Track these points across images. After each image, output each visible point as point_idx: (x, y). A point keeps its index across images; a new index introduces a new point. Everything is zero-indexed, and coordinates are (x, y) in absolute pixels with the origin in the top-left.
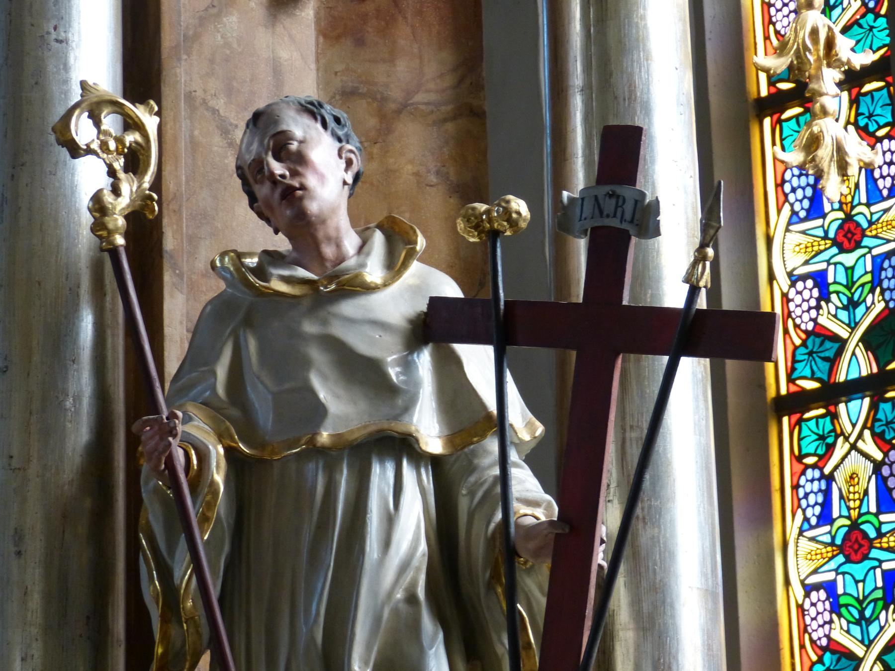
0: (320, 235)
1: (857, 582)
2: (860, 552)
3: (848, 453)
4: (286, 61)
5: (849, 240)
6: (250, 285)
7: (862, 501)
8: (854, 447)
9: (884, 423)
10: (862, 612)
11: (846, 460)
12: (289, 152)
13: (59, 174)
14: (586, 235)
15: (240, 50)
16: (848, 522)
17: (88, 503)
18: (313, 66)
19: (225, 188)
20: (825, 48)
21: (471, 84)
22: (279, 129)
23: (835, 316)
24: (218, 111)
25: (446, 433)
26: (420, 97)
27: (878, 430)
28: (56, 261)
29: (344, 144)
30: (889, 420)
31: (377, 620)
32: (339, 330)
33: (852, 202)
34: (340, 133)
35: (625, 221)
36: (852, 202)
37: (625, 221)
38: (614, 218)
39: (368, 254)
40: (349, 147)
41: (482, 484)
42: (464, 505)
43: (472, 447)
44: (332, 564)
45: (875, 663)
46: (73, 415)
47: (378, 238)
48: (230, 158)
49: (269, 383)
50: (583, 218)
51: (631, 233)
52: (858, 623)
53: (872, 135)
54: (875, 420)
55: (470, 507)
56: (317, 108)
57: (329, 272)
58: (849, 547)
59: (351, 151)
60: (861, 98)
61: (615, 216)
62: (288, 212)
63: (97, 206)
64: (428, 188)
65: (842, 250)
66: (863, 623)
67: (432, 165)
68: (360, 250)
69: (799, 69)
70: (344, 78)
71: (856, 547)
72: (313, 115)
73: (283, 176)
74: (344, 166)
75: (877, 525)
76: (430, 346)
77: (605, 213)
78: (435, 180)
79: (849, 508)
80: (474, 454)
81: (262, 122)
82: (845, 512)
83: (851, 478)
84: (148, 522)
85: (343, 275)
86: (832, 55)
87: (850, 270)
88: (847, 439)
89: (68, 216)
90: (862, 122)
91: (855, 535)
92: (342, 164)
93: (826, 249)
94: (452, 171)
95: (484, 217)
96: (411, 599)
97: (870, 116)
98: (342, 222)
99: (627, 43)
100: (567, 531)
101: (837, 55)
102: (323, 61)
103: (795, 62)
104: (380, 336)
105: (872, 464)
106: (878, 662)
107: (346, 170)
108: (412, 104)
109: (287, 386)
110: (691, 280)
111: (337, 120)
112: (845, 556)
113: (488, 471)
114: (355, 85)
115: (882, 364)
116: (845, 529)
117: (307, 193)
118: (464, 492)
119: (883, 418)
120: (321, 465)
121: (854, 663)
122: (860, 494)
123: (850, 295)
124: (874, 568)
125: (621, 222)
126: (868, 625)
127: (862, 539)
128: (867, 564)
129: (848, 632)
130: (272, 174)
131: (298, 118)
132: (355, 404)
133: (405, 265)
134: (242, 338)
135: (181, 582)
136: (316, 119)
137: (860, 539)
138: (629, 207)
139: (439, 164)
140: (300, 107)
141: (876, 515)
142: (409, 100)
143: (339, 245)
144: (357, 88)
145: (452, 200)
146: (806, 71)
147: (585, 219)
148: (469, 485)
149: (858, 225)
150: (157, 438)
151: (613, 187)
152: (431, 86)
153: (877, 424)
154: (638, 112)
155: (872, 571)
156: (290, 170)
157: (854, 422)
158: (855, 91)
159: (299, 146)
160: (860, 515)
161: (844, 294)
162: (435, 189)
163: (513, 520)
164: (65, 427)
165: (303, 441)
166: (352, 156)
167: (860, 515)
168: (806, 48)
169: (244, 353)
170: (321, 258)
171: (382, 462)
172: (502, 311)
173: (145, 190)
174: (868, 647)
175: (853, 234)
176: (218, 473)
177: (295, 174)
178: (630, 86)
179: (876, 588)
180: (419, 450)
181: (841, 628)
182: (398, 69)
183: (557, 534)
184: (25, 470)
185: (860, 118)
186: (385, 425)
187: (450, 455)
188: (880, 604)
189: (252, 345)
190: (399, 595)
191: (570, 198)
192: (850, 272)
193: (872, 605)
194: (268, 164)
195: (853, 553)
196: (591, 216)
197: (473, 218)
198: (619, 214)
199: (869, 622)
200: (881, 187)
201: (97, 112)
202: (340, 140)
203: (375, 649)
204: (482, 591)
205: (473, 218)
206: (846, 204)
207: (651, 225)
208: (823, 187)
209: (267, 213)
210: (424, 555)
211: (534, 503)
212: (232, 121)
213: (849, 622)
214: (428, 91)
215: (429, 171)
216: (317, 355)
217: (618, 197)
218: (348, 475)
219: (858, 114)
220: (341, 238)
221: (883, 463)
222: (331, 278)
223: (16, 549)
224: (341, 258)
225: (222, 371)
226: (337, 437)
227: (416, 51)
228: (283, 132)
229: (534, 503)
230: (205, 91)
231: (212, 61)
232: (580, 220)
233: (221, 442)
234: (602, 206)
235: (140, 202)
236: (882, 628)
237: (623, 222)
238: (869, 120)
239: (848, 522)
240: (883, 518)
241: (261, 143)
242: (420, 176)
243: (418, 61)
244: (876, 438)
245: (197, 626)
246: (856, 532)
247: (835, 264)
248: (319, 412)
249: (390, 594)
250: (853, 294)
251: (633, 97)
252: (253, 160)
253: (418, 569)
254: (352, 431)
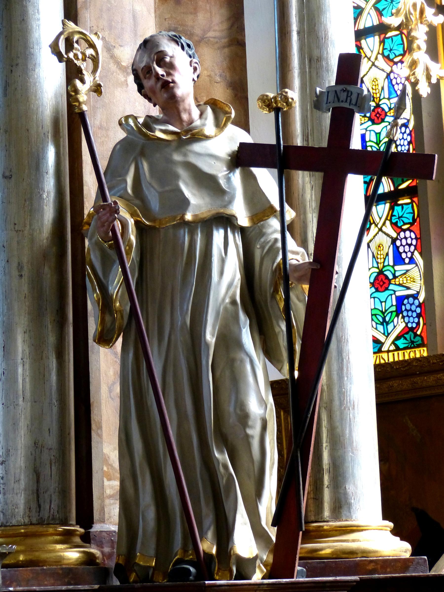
0: (181, 108)
1: (381, 302)
2: (383, 286)
3: (378, 233)
4: (139, 11)
5: (378, 118)
6: (145, 135)
7: (385, 259)
8: (380, 230)
9: (397, 217)
10: (384, 319)
11: (376, 236)
12: (165, 62)
13: (37, 70)
14: (330, 111)
15: (115, 5)
16: (377, 270)
17: (54, 249)
18: (153, 15)
19: (109, 81)
20: (419, 14)
21: (238, 27)
22: (160, 50)
23: (376, 329)
24: (105, 38)
25: (249, 215)
26: (211, 34)
27: (394, 221)
28: (36, 118)
29: (192, 59)
30: (400, 216)
31: (218, 313)
32: (193, 159)
33: (380, 97)
34: (190, 53)
35: (352, 104)
36: (380, 97)
37: (352, 104)
38: (346, 103)
39: (206, 119)
40: (195, 60)
41: (268, 242)
42: (258, 254)
43: (262, 223)
44: (194, 283)
45: (391, 345)
46: (48, 202)
47: (209, 111)
48: (112, 64)
49: (156, 186)
50: (328, 102)
51: (355, 111)
52: (382, 324)
53: (392, 60)
54: (392, 215)
55: (261, 255)
56: (179, 39)
57: (186, 128)
58: (377, 284)
59: (196, 63)
60: (386, 40)
61: (346, 101)
62: (165, 95)
63: (73, 89)
64: (215, 84)
65: (374, 123)
66: (385, 324)
67: (217, 72)
68: (201, 115)
69: (406, 25)
70: (170, 22)
71: (382, 283)
72: (177, 43)
73: (163, 75)
74: (193, 70)
75: (393, 272)
76: (239, 168)
77: (341, 100)
78: (219, 80)
79: (378, 263)
80: (263, 226)
81: (149, 46)
82: (375, 265)
83: (379, 246)
84: (90, 260)
85: (194, 130)
86: (423, 17)
87: (378, 134)
88: (376, 226)
89: (42, 94)
90: (386, 53)
91: (382, 277)
92: (192, 69)
93: (365, 123)
94: (228, 75)
95: (273, 100)
96: (233, 302)
97: (391, 50)
98: (190, 102)
99: (324, 8)
100: (319, 267)
101: (426, 18)
102: (158, 12)
103: (404, 21)
104: (215, 163)
105: (391, 239)
106: (392, 345)
107: (194, 73)
108: (207, 37)
109: (167, 188)
110: (390, 136)
111: (189, 46)
112: (375, 288)
113: (271, 236)
114: (176, 26)
115: (396, 186)
116: (376, 274)
117: (176, 85)
118: (258, 246)
119: (397, 215)
120: (187, 230)
121: (379, 345)
122: (384, 255)
123: (378, 148)
124: (391, 295)
125: (350, 105)
126: (387, 325)
127: (385, 279)
128: (387, 293)
129: (376, 329)
130: (157, 74)
131: (169, 44)
132: (204, 199)
133: (225, 125)
134: (140, 163)
135: (114, 293)
136: (178, 45)
137: (383, 279)
138: (354, 97)
139: (221, 71)
140: (169, 38)
141: (393, 267)
142: (205, 35)
143: (190, 114)
144: (177, 28)
145: (228, 91)
146: (409, 26)
147: (330, 103)
148: (261, 243)
149: (383, 110)
150: (108, 215)
151: (346, 86)
152: (217, 28)
153: (393, 218)
154: (330, 46)
155: (390, 296)
156: (166, 72)
157: (381, 217)
158: (382, 36)
159: (170, 59)
160: (384, 266)
161: (375, 147)
162: (219, 84)
163: (288, 262)
164: (43, 208)
165: (179, 218)
166: (196, 65)
167: (384, 266)
168: (410, 13)
169: (141, 171)
170: (181, 120)
171: (217, 230)
172: (282, 151)
173: (97, 81)
174: (387, 337)
175: (380, 115)
176: (132, 234)
177: (169, 74)
178: (325, 31)
179: (392, 305)
180: (236, 224)
181: (372, 326)
182: (199, 18)
183: (312, 269)
184: (23, 231)
185: (385, 51)
186: (222, 211)
187: (250, 227)
188: (394, 314)
189: (145, 166)
190: (227, 300)
191: (320, 92)
192: (378, 135)
193: (390, 314)
194: (154, 69)
195: (380, 287)
196: (333, 101)
197: (267, 101)
198: (348, 101)
199: (388, 323)
200: (396, 89)
201: (72, 37)
202: (190, 57)
203: (217, 328)
204: (269, 299)
205: (267, 101)
206: (377, 98)
207: (366, 106)
208: (418, 89)
209: (150, 95)
210: (239, 279)
211: (297, 253)
212: (112, 43)
213: (377, 323)
214: (214, 31)
215: (216, 75)
216: (182, 172)
217: (348, 91)
218: (201, 236)
219: (384, 49)
220: (191, 110)
221: (397, 239)
222: (187, 132)
223: (19, 273)
224: (191, 122)
225: (130, 180)
226: (195, 216)
227: (208, 8)
228: (162, 52)
229: (297, 253)
230: (98, 27)
231: (101, 10)
232: (327, 103)
233: (132, 217)
234: (339, 96)
235: (94, 88)
236: (395, 327)
237: (351, 105)
238: (390, 52)
239: (377, 270)
240: (397, 268)
241: (150, 57)
242: (211, 77)
243: (209, 14)
244: (393, 225)
245: (122, 317)
246: (381, 275)
247: (370, 131)
248: (185, 203)
249: (224, 300)
250: (380, 147)
251: (327, 37)
252: (145, 66)
253: (236, 287)
254: (202, 213)
